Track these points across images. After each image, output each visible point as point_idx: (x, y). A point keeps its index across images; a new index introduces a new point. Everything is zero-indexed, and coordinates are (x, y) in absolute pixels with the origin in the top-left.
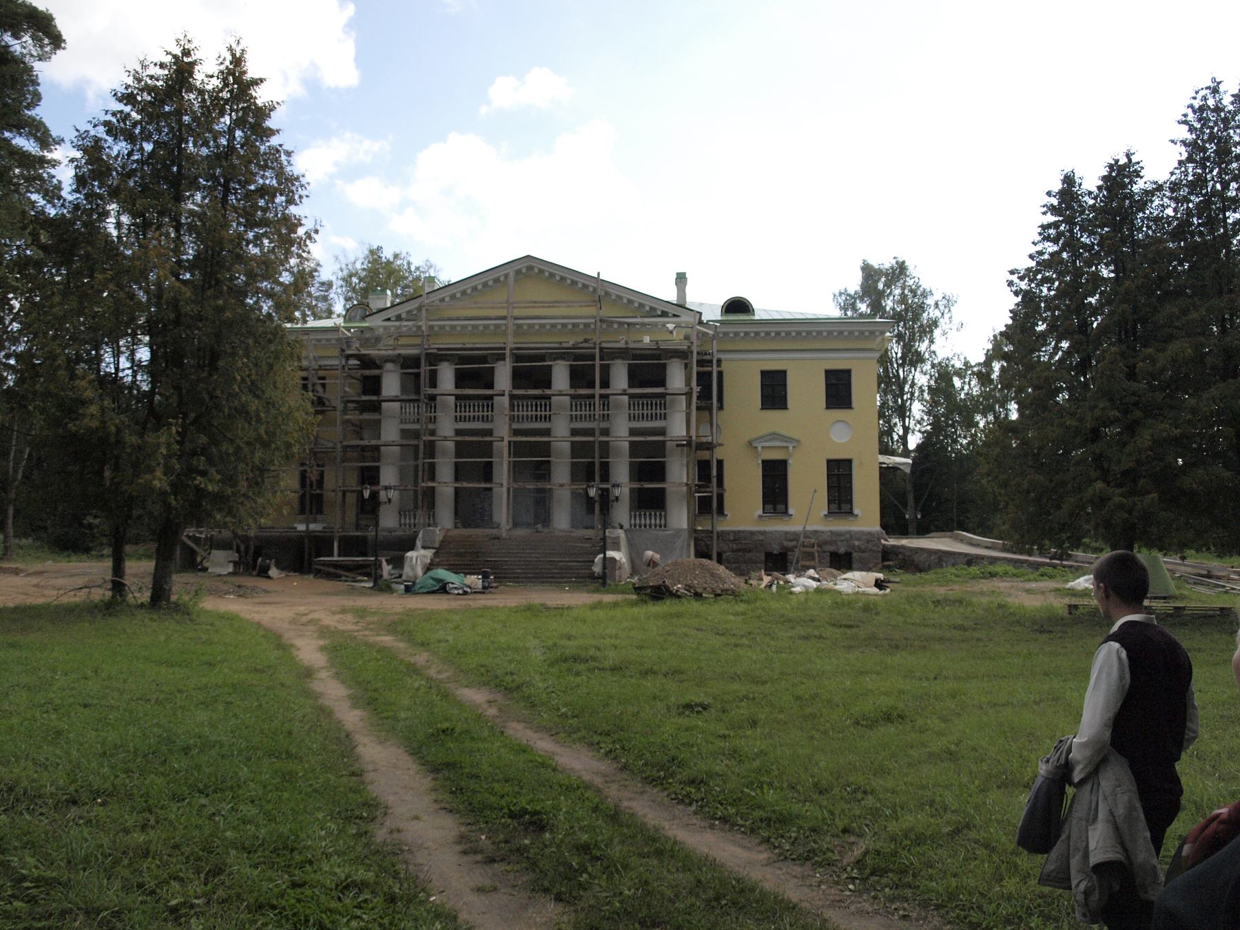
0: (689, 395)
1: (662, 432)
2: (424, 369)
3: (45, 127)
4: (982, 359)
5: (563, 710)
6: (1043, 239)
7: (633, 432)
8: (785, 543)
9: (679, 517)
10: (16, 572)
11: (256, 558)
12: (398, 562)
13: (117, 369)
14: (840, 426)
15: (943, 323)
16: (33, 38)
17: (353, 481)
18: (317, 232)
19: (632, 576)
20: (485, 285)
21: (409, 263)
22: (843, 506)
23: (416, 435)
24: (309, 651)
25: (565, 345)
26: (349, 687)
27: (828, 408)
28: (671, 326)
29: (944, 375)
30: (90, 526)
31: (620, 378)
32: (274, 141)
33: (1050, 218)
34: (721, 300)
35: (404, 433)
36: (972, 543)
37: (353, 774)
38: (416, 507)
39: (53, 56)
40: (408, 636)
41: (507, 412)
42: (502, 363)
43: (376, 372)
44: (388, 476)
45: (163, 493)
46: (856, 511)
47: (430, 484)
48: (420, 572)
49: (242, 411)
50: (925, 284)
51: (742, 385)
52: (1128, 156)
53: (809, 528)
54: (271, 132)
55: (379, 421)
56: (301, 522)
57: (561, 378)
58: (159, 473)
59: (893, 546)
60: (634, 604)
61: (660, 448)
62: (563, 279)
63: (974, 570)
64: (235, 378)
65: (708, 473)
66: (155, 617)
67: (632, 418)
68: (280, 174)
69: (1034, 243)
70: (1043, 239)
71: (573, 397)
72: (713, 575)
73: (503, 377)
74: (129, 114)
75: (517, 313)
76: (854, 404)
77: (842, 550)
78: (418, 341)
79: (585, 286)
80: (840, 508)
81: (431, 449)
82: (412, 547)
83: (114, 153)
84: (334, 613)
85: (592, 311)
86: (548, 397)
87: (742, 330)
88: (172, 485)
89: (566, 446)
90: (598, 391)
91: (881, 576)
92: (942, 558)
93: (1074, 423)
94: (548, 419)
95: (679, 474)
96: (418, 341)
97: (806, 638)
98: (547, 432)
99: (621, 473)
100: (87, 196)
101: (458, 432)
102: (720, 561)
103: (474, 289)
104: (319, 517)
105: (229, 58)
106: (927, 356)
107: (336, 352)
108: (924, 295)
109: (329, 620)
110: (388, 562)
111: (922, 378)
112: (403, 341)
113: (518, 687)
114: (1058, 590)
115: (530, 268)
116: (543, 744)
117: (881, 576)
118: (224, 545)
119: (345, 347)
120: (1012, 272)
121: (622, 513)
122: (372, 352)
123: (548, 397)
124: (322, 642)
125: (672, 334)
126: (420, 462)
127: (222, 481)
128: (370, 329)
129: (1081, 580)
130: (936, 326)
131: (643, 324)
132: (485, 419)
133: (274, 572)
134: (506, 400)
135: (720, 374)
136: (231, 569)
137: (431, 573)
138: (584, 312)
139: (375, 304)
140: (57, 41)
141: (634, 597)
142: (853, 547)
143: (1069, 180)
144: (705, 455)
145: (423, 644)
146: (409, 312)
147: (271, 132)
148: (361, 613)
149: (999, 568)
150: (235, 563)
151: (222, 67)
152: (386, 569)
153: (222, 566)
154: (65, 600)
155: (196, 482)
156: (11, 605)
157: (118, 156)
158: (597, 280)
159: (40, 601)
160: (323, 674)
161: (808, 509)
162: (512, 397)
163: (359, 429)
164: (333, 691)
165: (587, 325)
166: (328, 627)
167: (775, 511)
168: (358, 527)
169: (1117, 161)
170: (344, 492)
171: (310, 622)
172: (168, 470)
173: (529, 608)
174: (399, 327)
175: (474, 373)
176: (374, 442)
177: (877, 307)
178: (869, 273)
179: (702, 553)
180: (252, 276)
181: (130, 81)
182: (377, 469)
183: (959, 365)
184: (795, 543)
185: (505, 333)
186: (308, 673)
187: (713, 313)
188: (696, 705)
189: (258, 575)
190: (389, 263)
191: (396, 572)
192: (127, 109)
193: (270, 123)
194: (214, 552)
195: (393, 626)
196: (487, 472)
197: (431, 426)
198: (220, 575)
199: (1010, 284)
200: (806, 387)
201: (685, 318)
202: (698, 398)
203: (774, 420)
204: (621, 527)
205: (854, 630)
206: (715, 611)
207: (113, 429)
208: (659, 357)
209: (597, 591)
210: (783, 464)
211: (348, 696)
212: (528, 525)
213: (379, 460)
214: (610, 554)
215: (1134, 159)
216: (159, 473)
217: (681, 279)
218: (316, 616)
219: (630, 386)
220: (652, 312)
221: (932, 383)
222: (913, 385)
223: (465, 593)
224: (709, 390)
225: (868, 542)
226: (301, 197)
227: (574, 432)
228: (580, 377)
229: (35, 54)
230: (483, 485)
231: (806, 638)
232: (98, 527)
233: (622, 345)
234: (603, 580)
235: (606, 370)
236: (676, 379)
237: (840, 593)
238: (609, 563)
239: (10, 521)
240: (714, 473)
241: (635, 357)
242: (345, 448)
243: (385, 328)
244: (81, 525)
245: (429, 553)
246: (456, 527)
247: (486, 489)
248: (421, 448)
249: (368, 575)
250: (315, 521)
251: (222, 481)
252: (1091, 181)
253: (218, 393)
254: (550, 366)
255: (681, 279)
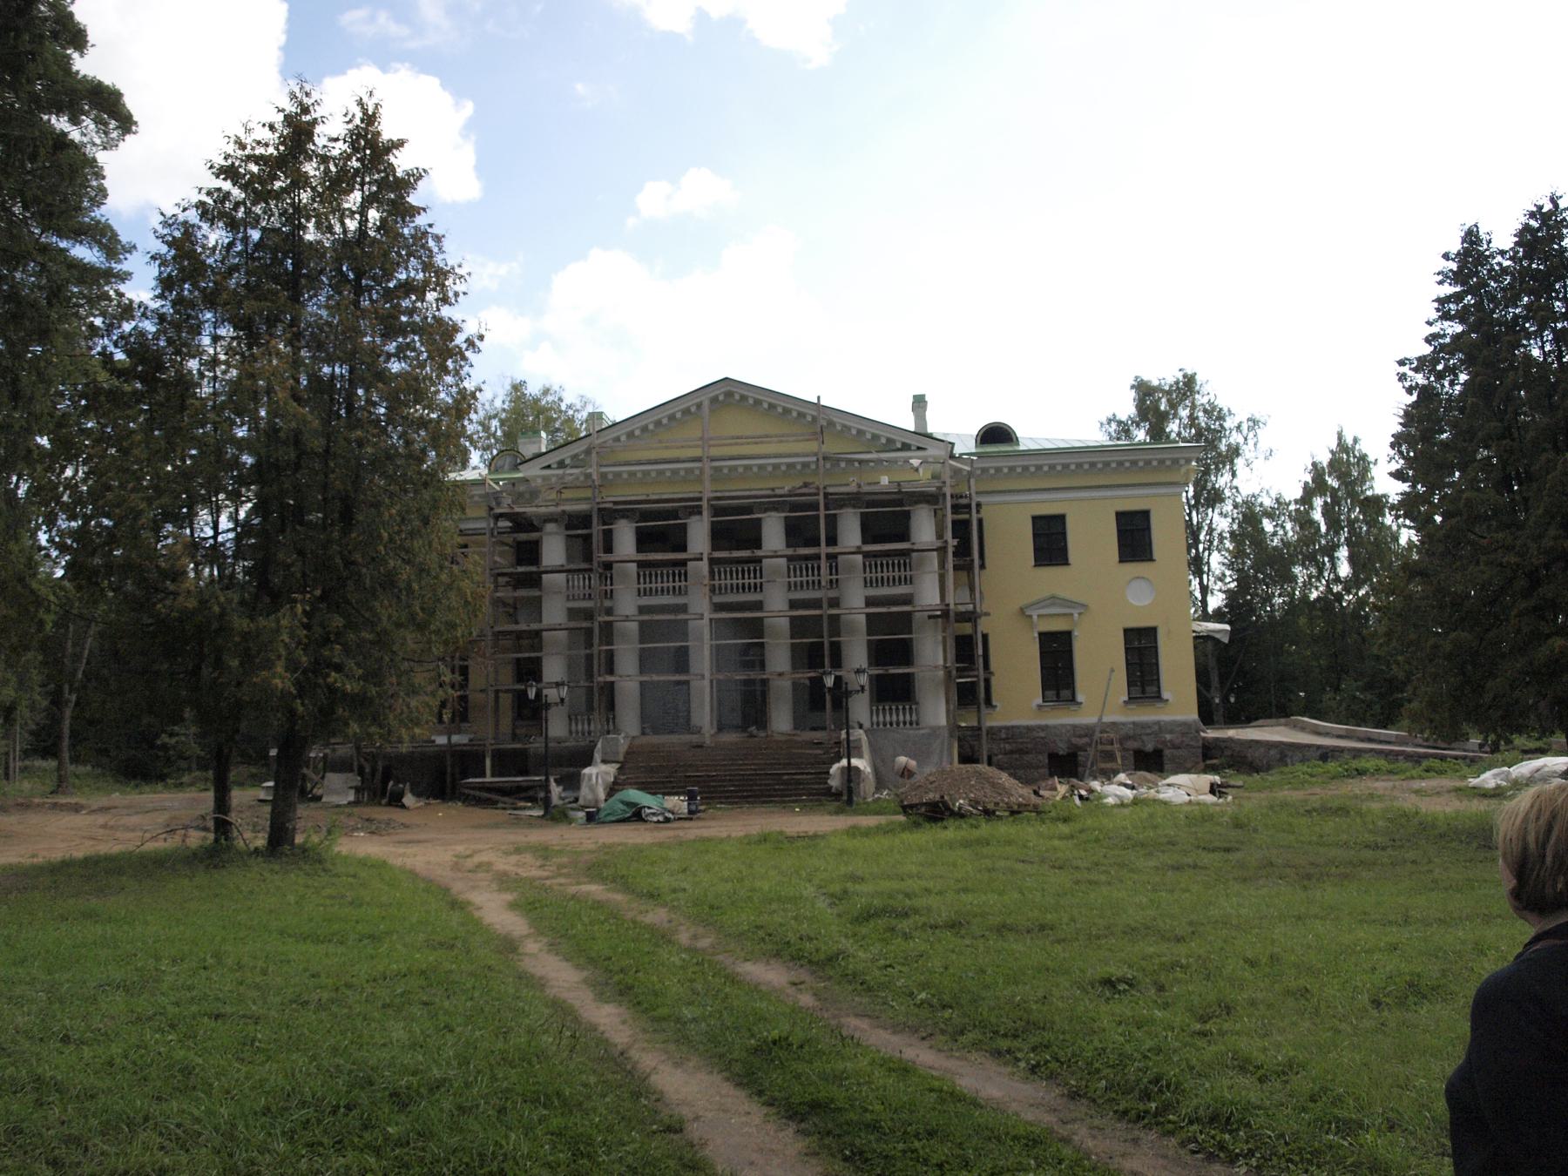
0: (942, 550)
1: (907, 600)
2: (597, 529)
3: (112, 230)
4: (1298, 494)
5: (923, 995)
6: (1441, 318)
7: (870, 602)
8: (1074, 740)
9: (935, 710)
10: (77, 809)
11: (383, 783)
12: (572, 782)
13: (217, 533)
15: (1247, 451)
16: (97, 121)
17: (507, 679)
18: (481, 338)
19: (879, 788)
20: (672, 417)
21: (561, 399)
22: (1148, 689)
23: (589, 615)
24: (496, 911)
25: (778, 492)
26: (578, 967)
27: (1151, 559)
28: (915, 462)
29: (1250, 516)
30: (165, 747)
31: (851, 533)
32: (421, 220)
33: (1448, 289)
34: (974, 429)
35: (573, 613)
36: (1317, 732)
37: (669, 1129)
38: (590, 708)
39: (121, 144)
40: (621, 882)
41: (706, 581)
42: (695, 518)
43: (534, 536)
44: (553, 669)
45: (284, 694)
46: (1165, 695)
47: (609, 678)
48: (602, 796)
49: (389, 582)
50: (1222, 403)
51: (1008, 533)
52: (1553, 200)
53: (1106, 719)
54: (414, 211)
55: (539, 599)
56: (440, 733)
57: (773, 534)
58: (279, 669)
59: (1217, 739)
60: (904, 828)
61: (905, 621)
62: (772, 406)
63: (1332, 766)
64: (380, 537)
65: (968, 651)
66: (277, 867)
67: (868, 583)
68: (428, 266)
69: (1430, 323)
70: (1441, 318)
71: (790, 559)
72: (993, 785)
73: (699, 536)
74: (229, 193)
75: (714, 452)
76: (1156, 555)
77: (1149, 747)
78: (588, 493)
79: (801, 415)
80: (1143, 692)
81: (608, 631)
82: (589, 762)
83: (211, 243)
84: (507, 853)
85: (813, 446)
86: (758, 560)
87: (1004, 464)
88: (297, 683)
89: (784, 623)
90: (824, 549)
91: (1217, 779)
92: (1285, 754)
93: (1514, 559)
94: (758, 588)
95: (932, 654)
96: (588, 493)
97: (1177, 868)
98: (758, 606)
99: (857, 654)
100: (174, 304)
101: (642, 610)
102: (990, 764)
103: (658, 423)
104: (465, 725)
105: (359, 115)
106: (1227, 493)
107: (483, 513)
108: (1221, 418)
109: (504, 864)
110: (558, 782)
111: (1221, 521)
112: (567, 494)
113: (830, 959)
114: (1457, 790)
115: (729, 394)
116: (923, 1056)
117: (1217, 779)
118: (342, 766)
119: (493, 504)
120: (1402, 363)
121: (860, 708)
122: (529, 510)
123: (758, 560)
124: (509, 897)
125: (918, 472)
126: (595, 649)
127: (364, 678)
128: (525, 480)
129: (1488, 774)
130: (1238, 455)
131: (880, 461)
132: (680, 592)
133: (409, 799)
134: (704, 566)
135: (980, 522)
136: (351, 798)
137: (619, 796)
138: (802, 448)
139: (527, 449)
140: (126, 124)
141: (902, 818)
142: (1164, 742)
143: (1472, 237)
144: (967, 628)
145: (651, 896)
146: (575, 457)
147: (414, 211)
148: (544, 852)
149: (1369, 763)
150: (358, 790)
151: (350, 126)
152: (556, 790)
153: (338, 793)
154: (150, 846)
155: (330, 680)
156: (79, 854)
157: (214, 248)
158: (817, 406)
159: (116, 849)
160: (532, 947)
161: (1101, 695)
162: (712, 561)
163: (512, 610)
164: (562, 977)
165: (805, 465)
166: (505, 874)
167: (1058, 699)
168: (515, 737)
169: (1541, 207)
170: (497, 692)
171: (479, 866)
172: (292, 665)
173: (764, 839)
174: (562, 477)
175: (661, 533)
176: (534, 626)
177: (1157, 432)
178: (1144, 391)
179: (967, 758)
180: (394, 406)
181: (231, 148)
182: (538, 661)
183: (1268, 503)
184: (1085, 740)
185: (699, 480)
186: (509, 946)
187: (966, 445)
188: (1120, 980)
189: (389, 804)
190: (537, 401)
191: (570, 795)
192: (227, 186)
193: (413, 199)
194: (330, 776)
195: (596, 869)
196: (681, 661)
197: (607, 603)
198: (338, 806)
199: (1402, 377)
200: (1091, 535)
201: (933, 451)
202: (955, 554)
203: (1052, 579)
204: (861, 727)
205: (1238, 855)
206: (1029, 831)
207: (216, 609)
208: (900, 503)
209: (838, 812)
211: (585, 981)
212: (736, 728)
213: (540, 649)
214: (854, 762)
215: (1562, 204)
216: (279, 669)
217: (919, 403)
218: (484, 858)
219: (865, 542)
220: (890, 445)
221: (1235, 527)
222: (1211, 530)
223: (667, 820)
224: (966, 545)
225: (1183, 734)
226: (456, 294)
227: (793, 604)
228: (798, 532)
229: (98, 141)
230: (677, 678)
231: (1177, 868)
232: (174, 747)
233: (853, 488)
234: (846, 797)
235: (832, 522)
236: (924, 529)
237: (1165, 803)
238: (851, 773)
239: (66, 743)
240: (980, 652)
241: (870, 504)
242: (497, 635)
243: (545, 478)
244: (152, 746)
245: (611, 769)
246: (643, 733)
247: (678, 683)
249: (533, 800)
250: (459, 732)
251: (364, 678)
252: (1502, 237)
253: (357, 557)
254: (760, 520)
255: (919, 403)
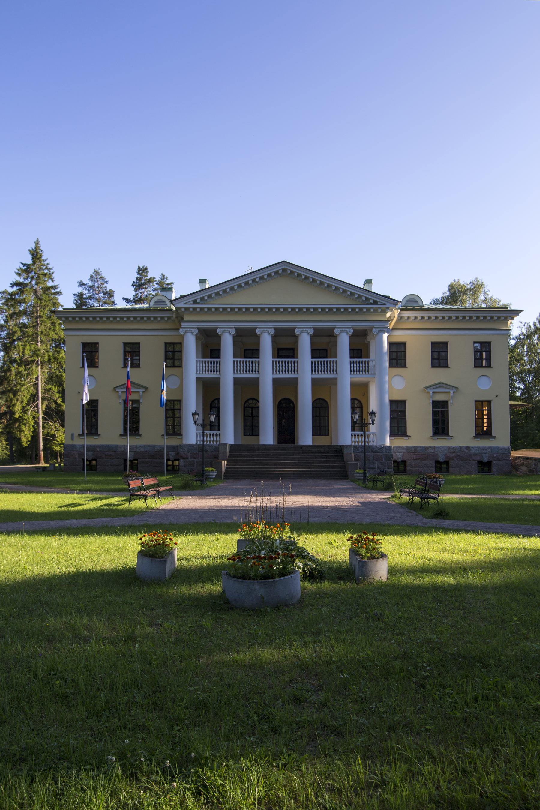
8: (448, 455)
14: (484, 379)
210: (445, 404)
248: (210, 392)
